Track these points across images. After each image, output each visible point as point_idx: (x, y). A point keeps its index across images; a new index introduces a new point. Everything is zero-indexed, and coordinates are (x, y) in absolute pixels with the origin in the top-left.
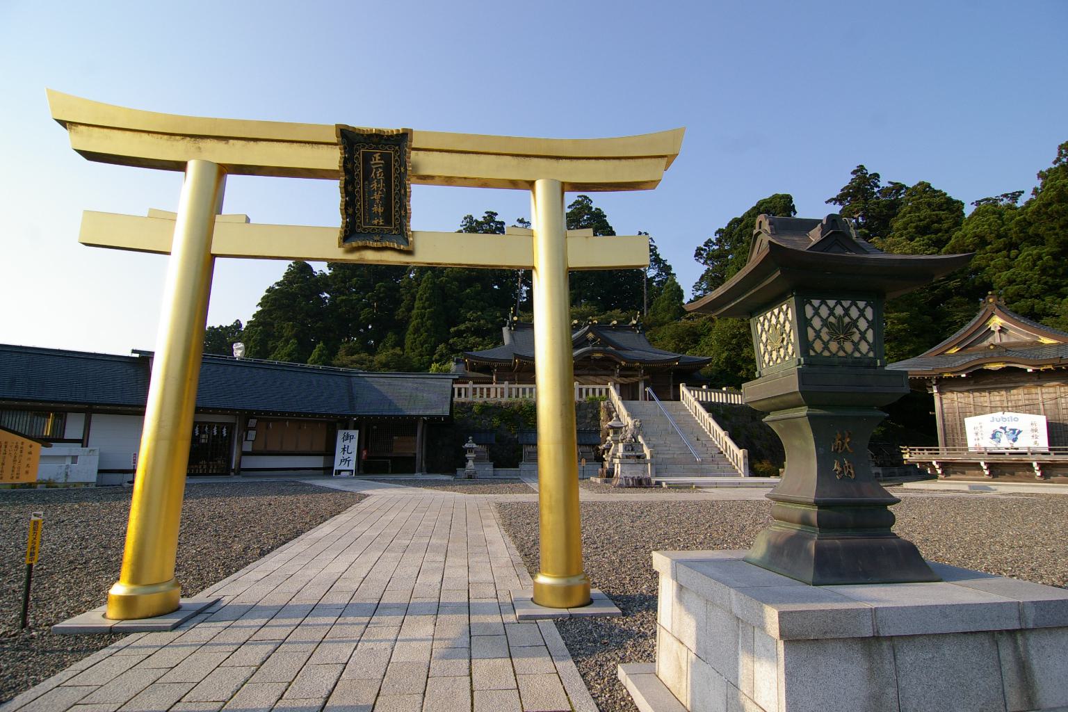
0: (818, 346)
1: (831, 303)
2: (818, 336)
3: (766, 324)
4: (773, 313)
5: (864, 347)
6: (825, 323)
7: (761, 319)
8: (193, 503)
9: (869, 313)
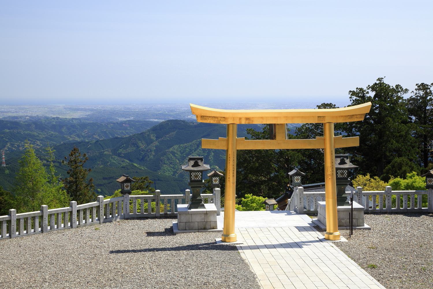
0: (339, 176)
2: (339, 174)
6: (340, 173)
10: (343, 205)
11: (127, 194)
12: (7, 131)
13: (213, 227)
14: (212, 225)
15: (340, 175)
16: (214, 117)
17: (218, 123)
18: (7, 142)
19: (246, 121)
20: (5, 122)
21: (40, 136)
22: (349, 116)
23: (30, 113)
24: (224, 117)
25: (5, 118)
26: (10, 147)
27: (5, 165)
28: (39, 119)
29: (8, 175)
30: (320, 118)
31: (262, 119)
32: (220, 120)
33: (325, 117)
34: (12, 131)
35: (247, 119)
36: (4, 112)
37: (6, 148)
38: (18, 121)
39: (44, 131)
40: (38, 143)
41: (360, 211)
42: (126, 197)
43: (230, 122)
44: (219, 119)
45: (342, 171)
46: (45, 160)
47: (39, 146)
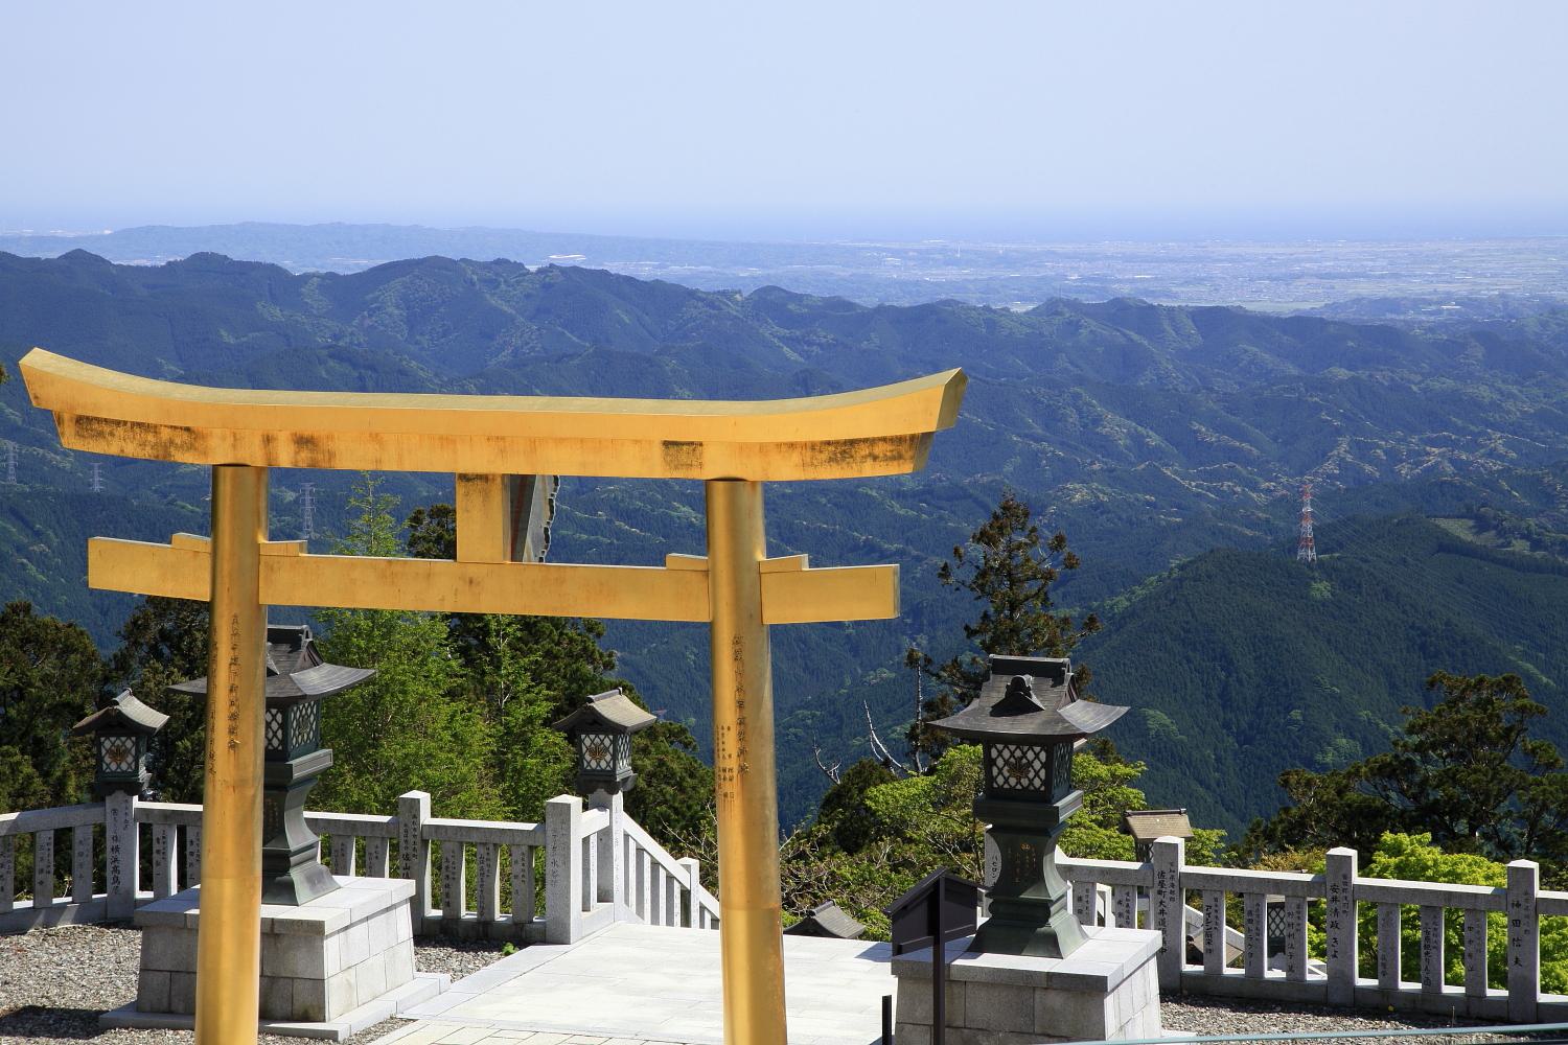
0: (1000, 780)
1: (592, 736)
2: (1000, 771)
3: (298, 713)
4: (298, 708)
5: (1037, 783)
6: (1006, 762)
7: (295, 708)
8: (499, 480)
9: (1043, 756)
10: (1017, 951)
11: (120, 795)
12: (1342, 373)
13: (306, 1012)
14: (302, 999)
15: (1007, 774)
16: (140, 425)
17: (161, 458)
18: (1338, 432)
19: (297, 453)
20: (1331, 329)
21: (1509, 405)
22: (829, 443)
23: (1463, 282)
24: (188, 429)
25: (1334, 307)
26: (1349, 458)
27: (1311, 554)
28: (1512, 317)
29: (1323, 605)
30: (673, 450)
31: (377, 447)
32: (172, 442)
33: (701, 444)
34: (1363, 374)
35: (303, 441)
36: (1334, 277)
37: (1330, 467)
38: (1398, 325)
39: (1534, 381)
40: (1498, 442)
41: (1083, 993)
42: (115, 811)
43: (219, 452)
44: (165, 434)
45: (1018, 753)
46: (1523, 537)
47: (1501, 457)
